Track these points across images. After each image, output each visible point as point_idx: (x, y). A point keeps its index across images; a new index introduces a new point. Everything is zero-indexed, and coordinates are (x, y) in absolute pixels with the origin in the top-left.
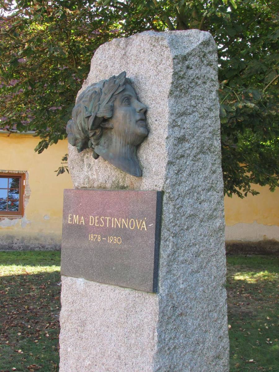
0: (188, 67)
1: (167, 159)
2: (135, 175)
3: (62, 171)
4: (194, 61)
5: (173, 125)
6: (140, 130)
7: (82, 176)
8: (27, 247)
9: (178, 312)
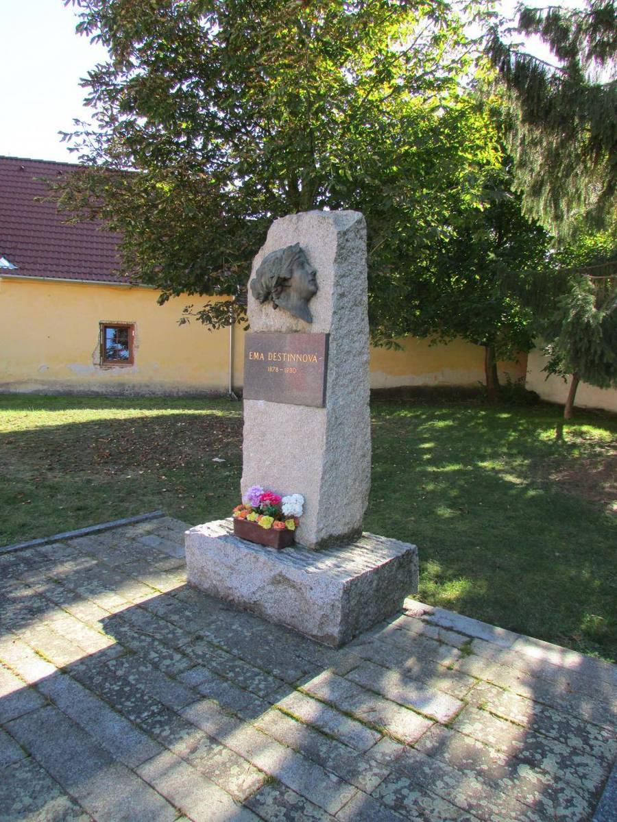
0: (347, 240)
1: (333, 310)
2: (308, 322)
3: (183, 322)
4: (351, 235)
5: (337, 284)
6: (312, 288)
7: (261, 323)
8: (138, 393)
9: (339, 422)
